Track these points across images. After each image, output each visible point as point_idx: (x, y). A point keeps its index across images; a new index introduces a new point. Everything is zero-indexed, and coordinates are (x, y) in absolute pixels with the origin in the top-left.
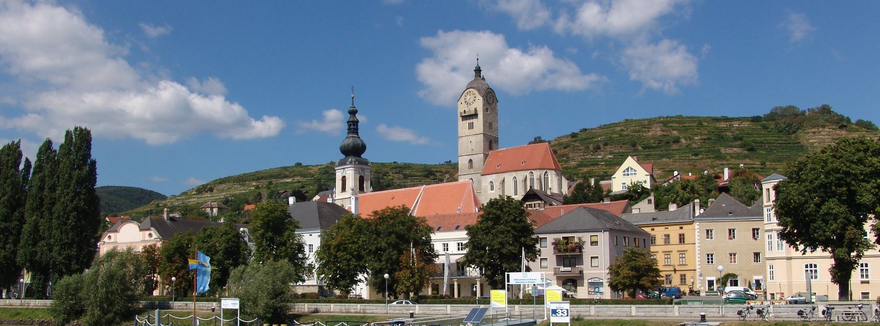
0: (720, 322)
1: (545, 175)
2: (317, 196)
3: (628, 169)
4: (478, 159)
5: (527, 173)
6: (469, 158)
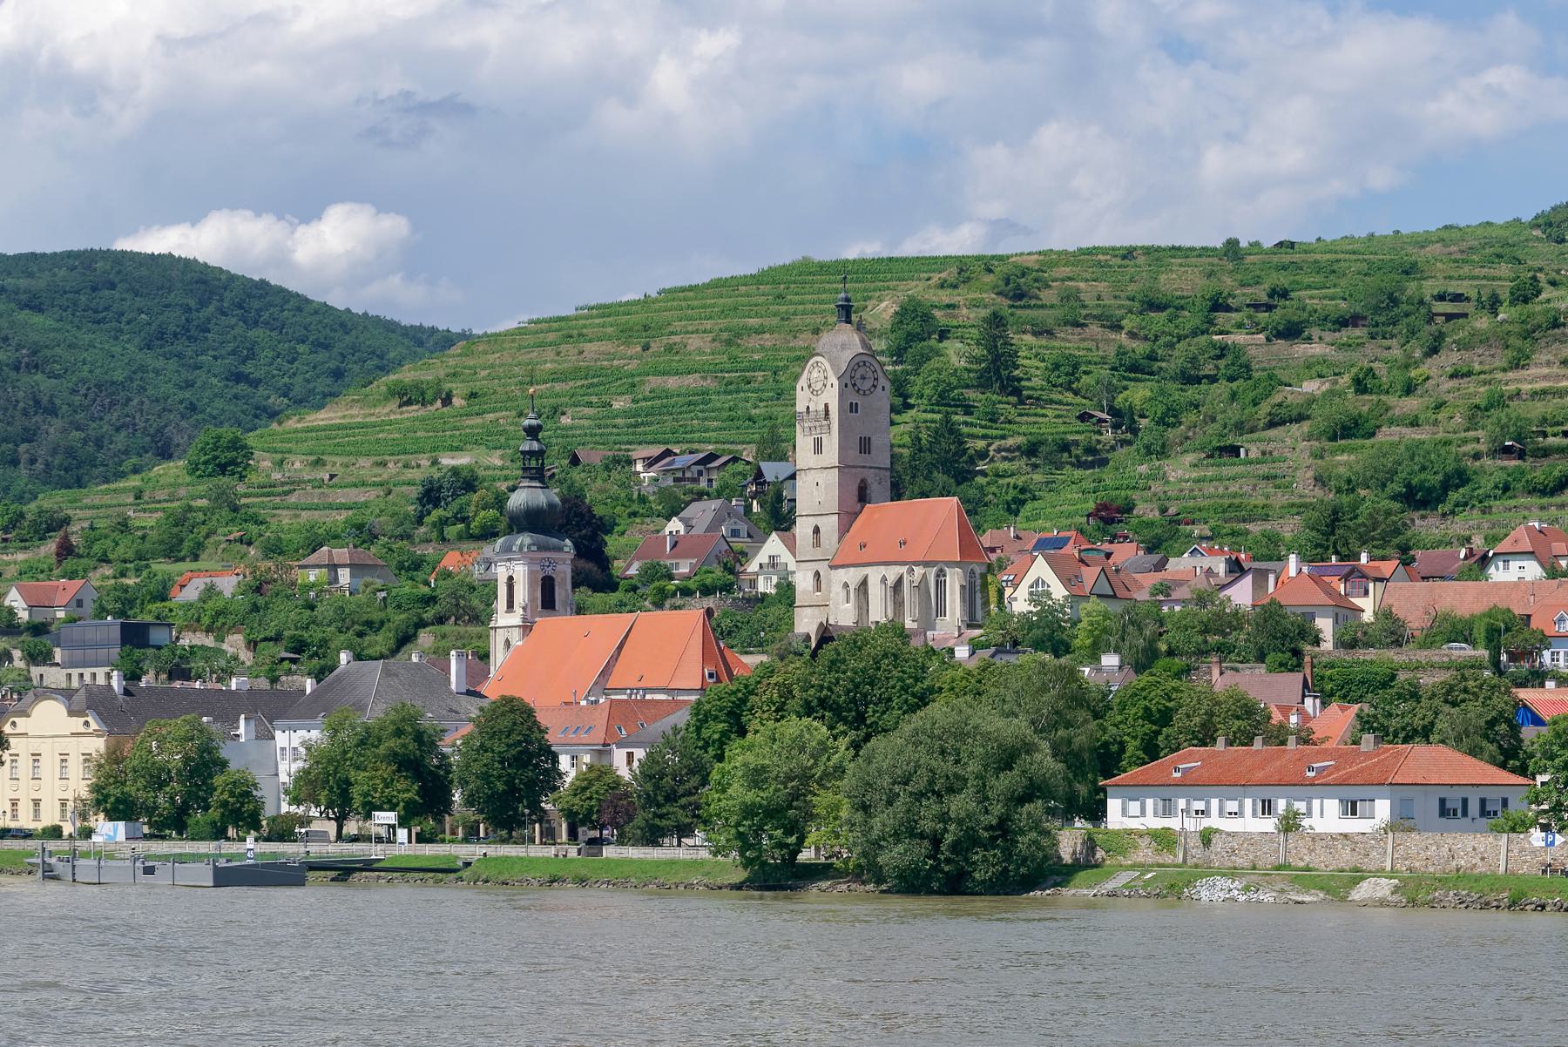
0: (337, 873)
1: (938, 576)
2: (674, 518)
3: (1037, 582)
4: (830, 524)
5: (904, 569)
6: (812, 521)
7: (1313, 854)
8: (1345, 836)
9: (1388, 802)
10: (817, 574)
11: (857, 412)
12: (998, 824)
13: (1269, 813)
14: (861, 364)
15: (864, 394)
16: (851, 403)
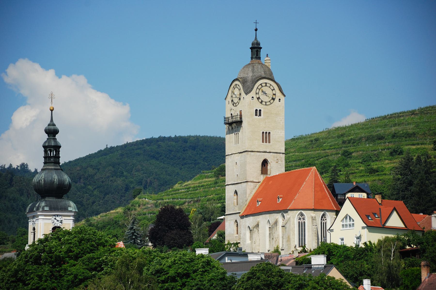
3: (346, 217)
9: (32, 171)
11: (260, 115)
14: (264, 85)
15: (266, 105)
16: (256, 110)
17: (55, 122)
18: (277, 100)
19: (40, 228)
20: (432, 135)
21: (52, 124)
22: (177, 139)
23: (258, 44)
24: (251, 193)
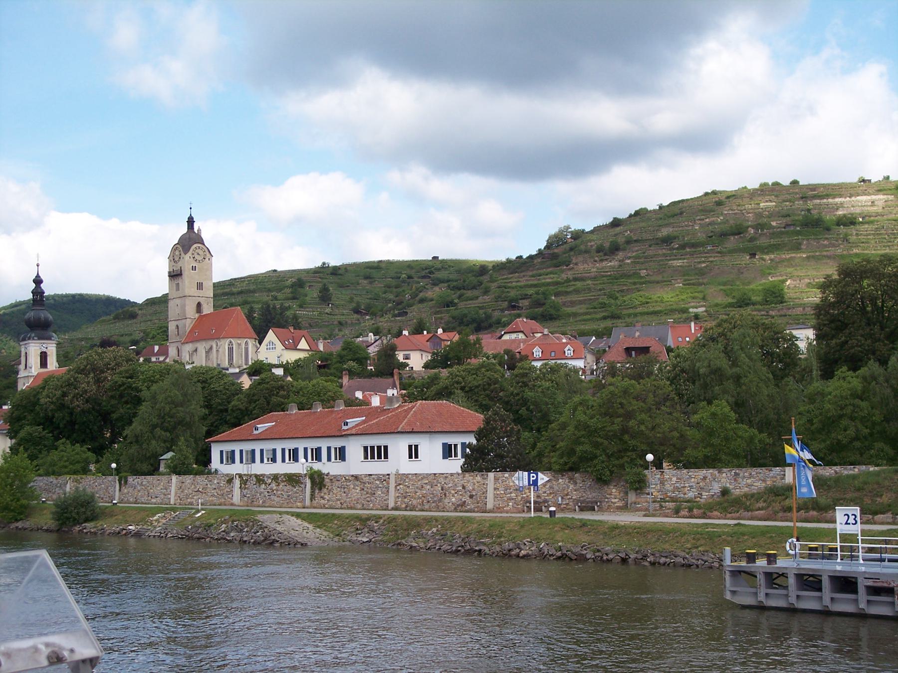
7: (331, 493)
8: (356, 477)
10: (178, 347)
11: (195, 270)
12: (745, 458)
13: (373, 457)
17: (40, 274)
18: (207, 259)
19: (586, 296)
20: (126, 304)
21: (38, 276)
22: (67, 296)
23: (192, 218)
24: (189, 327)
